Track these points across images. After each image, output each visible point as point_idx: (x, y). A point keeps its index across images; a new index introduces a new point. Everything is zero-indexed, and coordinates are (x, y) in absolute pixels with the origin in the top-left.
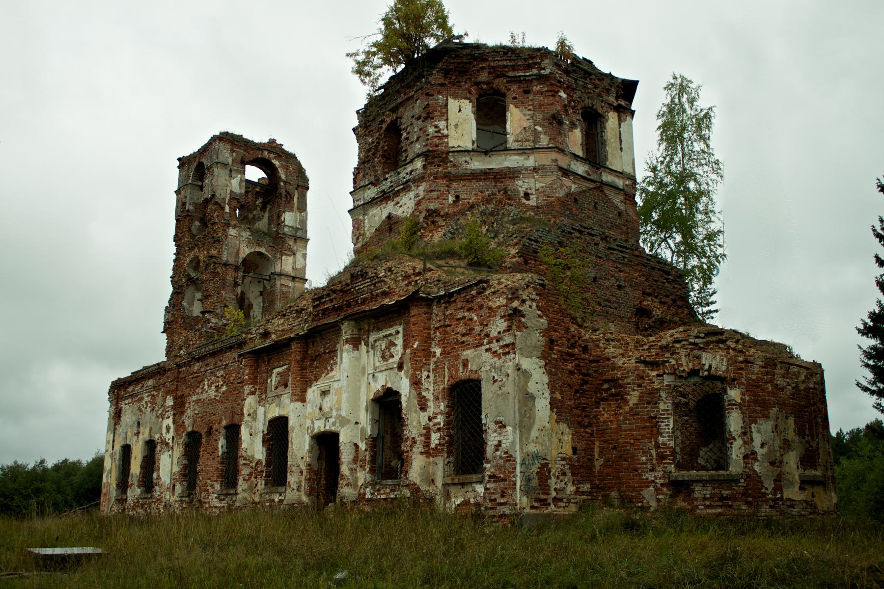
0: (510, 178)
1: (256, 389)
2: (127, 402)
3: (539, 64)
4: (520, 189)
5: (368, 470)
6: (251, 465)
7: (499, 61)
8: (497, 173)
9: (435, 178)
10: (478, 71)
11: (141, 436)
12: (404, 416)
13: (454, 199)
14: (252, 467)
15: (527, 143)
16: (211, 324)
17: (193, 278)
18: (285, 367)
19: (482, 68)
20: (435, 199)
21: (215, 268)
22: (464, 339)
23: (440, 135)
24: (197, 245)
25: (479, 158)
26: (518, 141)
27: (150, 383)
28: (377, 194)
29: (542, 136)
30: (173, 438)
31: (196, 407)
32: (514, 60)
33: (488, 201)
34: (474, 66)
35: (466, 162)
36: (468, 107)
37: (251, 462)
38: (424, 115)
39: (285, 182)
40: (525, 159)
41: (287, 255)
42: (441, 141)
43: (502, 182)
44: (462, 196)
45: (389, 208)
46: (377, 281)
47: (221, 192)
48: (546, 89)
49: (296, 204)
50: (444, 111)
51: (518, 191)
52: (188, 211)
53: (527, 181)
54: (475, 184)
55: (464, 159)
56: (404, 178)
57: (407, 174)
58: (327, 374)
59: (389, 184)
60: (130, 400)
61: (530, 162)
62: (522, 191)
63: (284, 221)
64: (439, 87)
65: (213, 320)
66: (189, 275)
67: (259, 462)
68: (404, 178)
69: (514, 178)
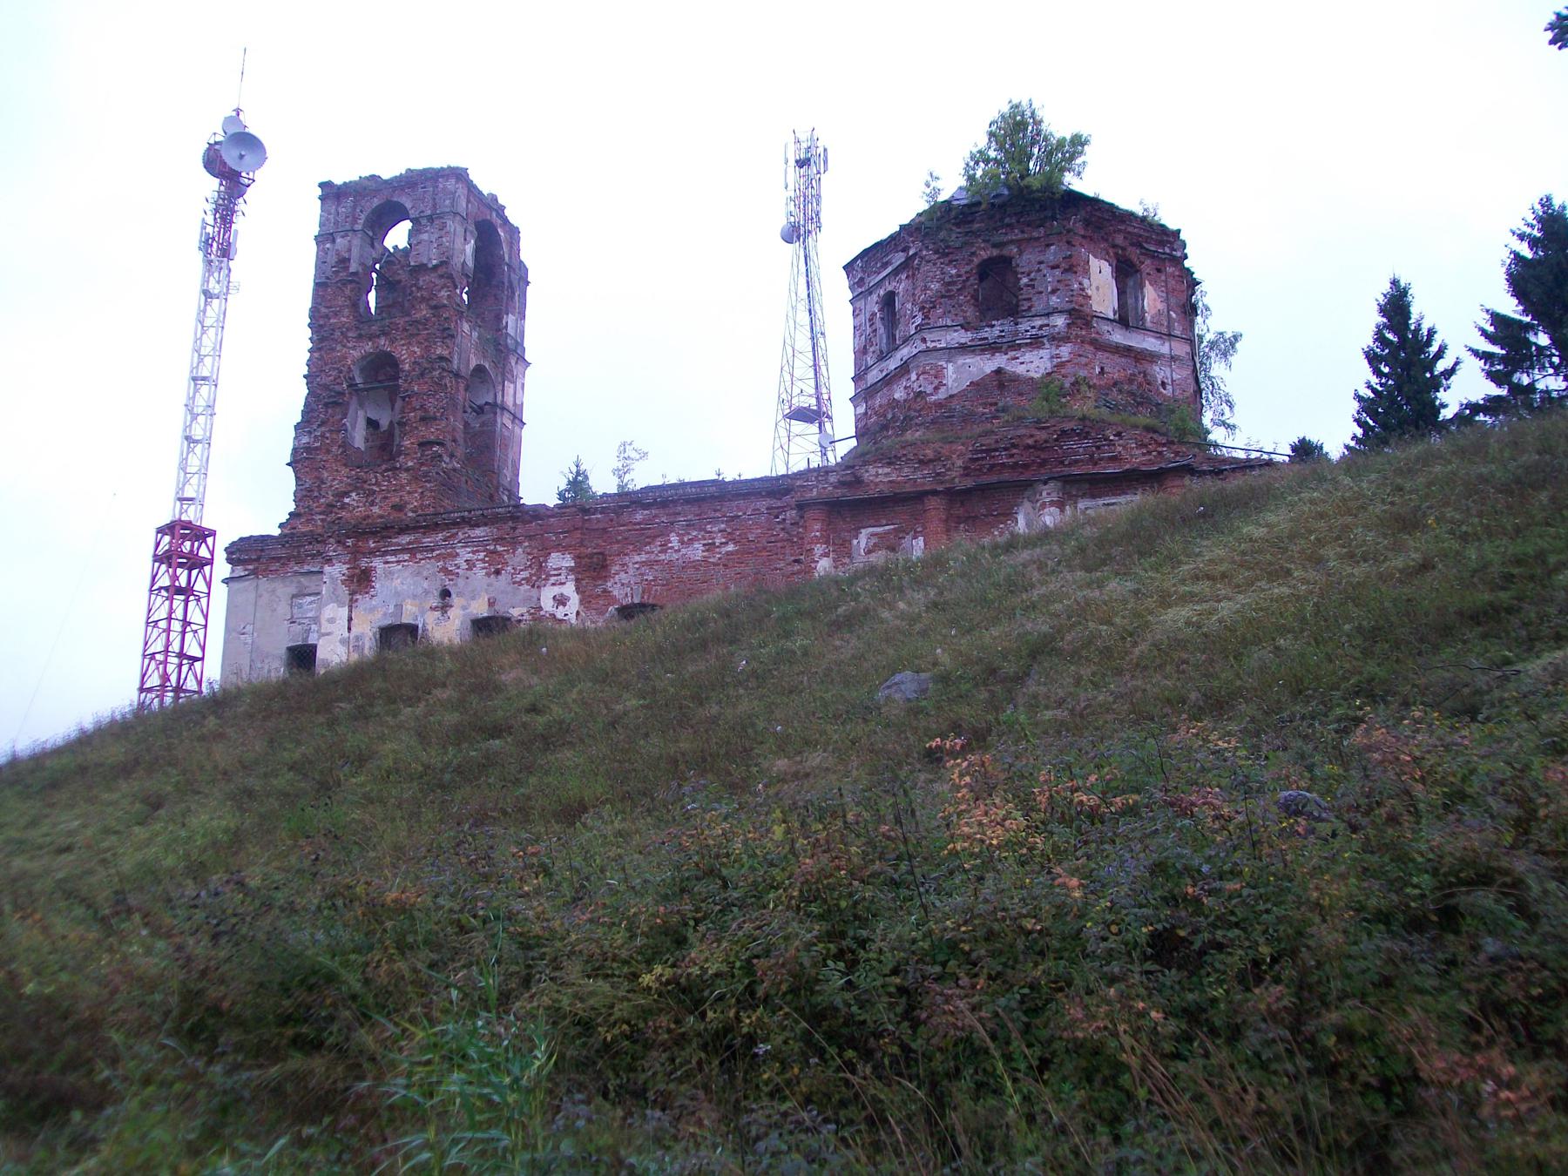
2: (390, 558)
9: (1082, 342)
19: (1120, 231)
21: (442, 378)
28: (972, 340)
30: (578, 613)
33: (1131, 381)
36: (1107, 269)
44: (1106, 369)
45: (999, 361)
57: (1033, 327)
59: (997, 333)
61: (1164, 349)
62: (1159, 378)
66: (353, 379)
69: (1152, 362)
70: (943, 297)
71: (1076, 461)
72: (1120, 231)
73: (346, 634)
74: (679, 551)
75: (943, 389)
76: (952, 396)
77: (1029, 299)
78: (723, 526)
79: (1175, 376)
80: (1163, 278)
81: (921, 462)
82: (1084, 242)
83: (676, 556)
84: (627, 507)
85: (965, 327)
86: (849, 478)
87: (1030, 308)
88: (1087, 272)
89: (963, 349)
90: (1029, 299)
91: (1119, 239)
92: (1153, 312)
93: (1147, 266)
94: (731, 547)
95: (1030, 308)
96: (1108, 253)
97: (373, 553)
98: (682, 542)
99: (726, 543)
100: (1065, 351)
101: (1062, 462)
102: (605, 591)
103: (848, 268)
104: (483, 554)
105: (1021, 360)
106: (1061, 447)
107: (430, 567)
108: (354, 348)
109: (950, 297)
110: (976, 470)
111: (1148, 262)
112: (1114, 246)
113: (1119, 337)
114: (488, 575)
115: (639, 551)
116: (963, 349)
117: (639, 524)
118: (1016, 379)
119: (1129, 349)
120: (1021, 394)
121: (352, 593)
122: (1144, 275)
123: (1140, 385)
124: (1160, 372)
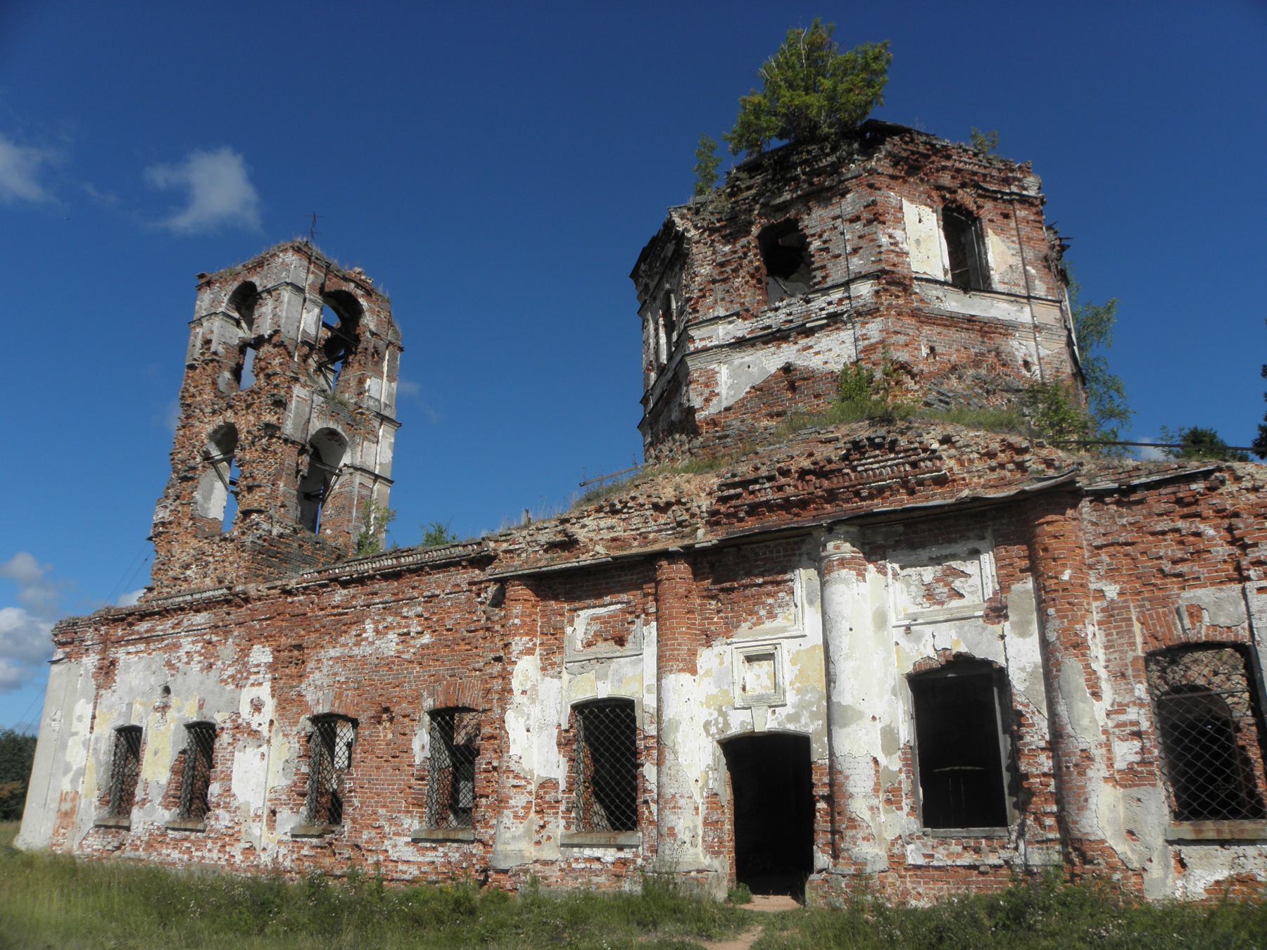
0: (1001, 334)
1: (535, 645)
2: (131, 649)
3: (1019, 180)
4: (1016, 353)
5: (906, 809)
6: (529, 788)
7: (966, 163)
8: (986, 323)
10: (938, 171)
11: (171, 714)
12: (1020, 708)
13: (928, 351)
14: (530, 793)
15: (1016, 288)
16: (260, 532)
17: (213, 458)
18: (619, 606)
19: (944, 168)
20: (902, 346)
22: (1180, 568)
23: (898, 250)
24: (231, 407)
25: (957, 297)
26: (1004, 283)
27: (201, 618)
28: (752, 332)
29: (1037, 282)
30: (272, 722)
31: (339, 669)
32: (985, 167)
34: (933, 162)
35: (938, 298)
37: (529, 783)
38: (865, 215)
39: (373, 334)
40: (1018, 311)
41: (370, 441)
42: (901, 259)
43: (990, 338)
44: (939, 349)
45: (788, 353)
46: (919, 455)
47: (290, 328)
48: (1032, 218)
49: (385, 369)
50: (900, 215)
51: (1014, 356)
52: (215, 353)
53: (1024, 343)
54: (953, 334)
55: (935, 293)
56: (822, 309)
57: (830, 303)
58: (755, 624)
60: (142, 647)
61: (1024, 315)
63: (369, 390)
64: (887, 179)
65: (265, 526)
67: (547, 784)
68: (822, 309)
70: (714, 282)
71: (881, 491)
72: (944, 168)
73: (88, 735)
74: (373, 643)
75: (715, 401)
76: (727, 409)
77: (823, 267)
78: (419, 609)
79: (1043, 352)
80: (1013, 224)
81: (656, 507)
82: (893, 183)
83: (369, 650)
84: (326, 586)
85: (743, 314)
86: (560, 538)
87: (824, 278)
88: (899, 221)
89: (740, 343)
90: (823, 267)
91: (946, 179)
92: (1003, 268)
93: (988, 210)
94: (426, 639)
95: (824, 278)
96: (929, 197)
97: (118, 642)
98: (377, 631)
99: (421, 633)
100: (874, 329)
101: (857, 494)
102: (300, 695)
103: (631, 276)
104: (201, 644)
105: (816, 349)
106: (854, 469)
107: (159, 658)
108: (209, 423)
109: (724, 281)
110: (728, 516)
111: (989, 205)
112: (939, 188)
113: (956, 303)
114: (202, 670)
115: (334, 642)
116: (740, 343)
117: (338, 607)
118: (810, 376)
119: (971, 320)
120: (817, 396)
121: (99, 687)
122: (985, 223)
123: (993, 368)
124: (1021, 348)
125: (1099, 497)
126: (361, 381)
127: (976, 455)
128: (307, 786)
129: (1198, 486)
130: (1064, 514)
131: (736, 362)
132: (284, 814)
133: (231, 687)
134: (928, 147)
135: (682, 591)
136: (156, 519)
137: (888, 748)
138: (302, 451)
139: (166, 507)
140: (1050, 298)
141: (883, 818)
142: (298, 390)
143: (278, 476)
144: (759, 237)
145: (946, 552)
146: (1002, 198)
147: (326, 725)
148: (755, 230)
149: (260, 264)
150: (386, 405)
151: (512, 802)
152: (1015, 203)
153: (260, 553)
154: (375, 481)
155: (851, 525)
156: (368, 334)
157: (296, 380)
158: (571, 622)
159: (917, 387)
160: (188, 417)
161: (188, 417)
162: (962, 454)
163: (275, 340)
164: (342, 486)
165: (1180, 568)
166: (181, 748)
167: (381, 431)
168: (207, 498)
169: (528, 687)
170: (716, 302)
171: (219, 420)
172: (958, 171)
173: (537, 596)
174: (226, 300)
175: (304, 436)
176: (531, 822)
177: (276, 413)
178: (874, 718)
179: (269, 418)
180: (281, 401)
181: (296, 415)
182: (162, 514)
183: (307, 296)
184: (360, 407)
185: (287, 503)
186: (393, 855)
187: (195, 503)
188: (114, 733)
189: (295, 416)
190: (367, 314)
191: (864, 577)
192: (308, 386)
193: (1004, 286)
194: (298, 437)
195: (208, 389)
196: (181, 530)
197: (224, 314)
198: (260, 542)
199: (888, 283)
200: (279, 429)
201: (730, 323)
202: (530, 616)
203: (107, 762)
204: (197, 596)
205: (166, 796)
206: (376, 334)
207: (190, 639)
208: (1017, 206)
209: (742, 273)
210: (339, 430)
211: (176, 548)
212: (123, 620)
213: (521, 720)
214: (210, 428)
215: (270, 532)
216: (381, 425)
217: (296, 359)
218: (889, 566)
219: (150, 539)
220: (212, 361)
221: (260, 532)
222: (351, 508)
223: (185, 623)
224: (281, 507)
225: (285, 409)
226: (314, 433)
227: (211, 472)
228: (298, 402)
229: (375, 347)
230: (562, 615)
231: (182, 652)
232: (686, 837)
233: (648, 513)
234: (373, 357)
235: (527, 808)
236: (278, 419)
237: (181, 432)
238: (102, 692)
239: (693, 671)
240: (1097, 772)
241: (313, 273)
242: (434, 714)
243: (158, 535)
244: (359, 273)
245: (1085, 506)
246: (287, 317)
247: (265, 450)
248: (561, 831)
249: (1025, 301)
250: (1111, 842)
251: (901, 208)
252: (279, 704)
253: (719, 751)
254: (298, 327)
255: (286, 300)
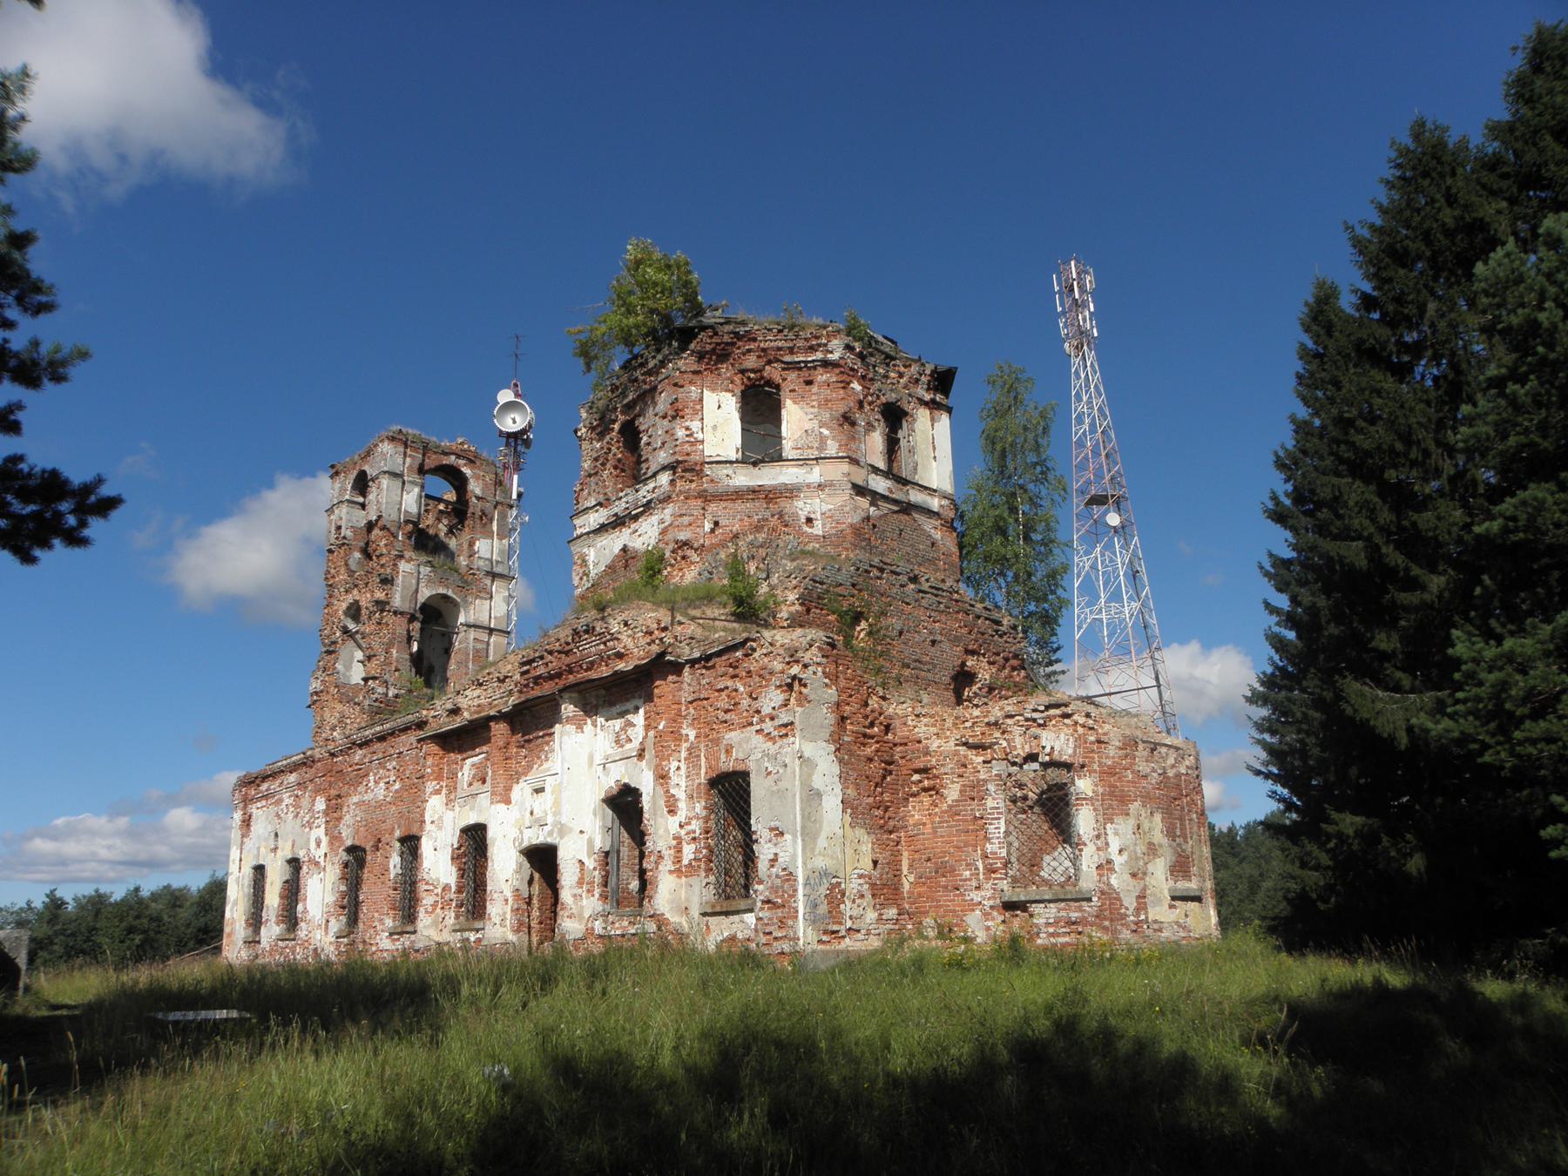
2: (259, 805)
4: (800, 512)
5: (597, 896)
6: (436, 891)
7: (771, 341)
10: (744, 354)
11: (279, 852)
14: (437, 895)
16: (376, 695)
19: (749, 351)
20: (686, 526)
22: (728, 717)
24: (356, 586)
32: (792, 340)
39: (478, 498)
40: (807, 472)
41: (482, 598)
49: (495, 528)
53: (809, 501)
55: (725, 471)
60: (264, 803)
61: (815, 475)
64: (690, 376)
65: (381, 690)
67: (446, 888)
68: (644, 497)
72: (749, 351)
89: (602, 529)
125: (693, 663)
126: (471, 544)
127: (641, 634)
128: (345, 900)
129: (739, 654)
130: (665, 680)
131: (599, 545)
132: (333, 921)
133: (308, 829)
134: (732, 336)
135: (501, 744)
136: (311, 689)
137: (591, 852)
138: (412, 619)
139: (317, 678)
140: (840, 455)
141: (585, 902)
142: (403, 566)
143: (389, 645)
144: (621, 431)
145: (624, 709)
146: (806, 366)
147: (355, 851)
148: (616, 426)
149: (368, 454)
150: (497, 562)
151: (424, 902)
152: (819, 368)
153: (377, 713)
154: (490, 634)
155: (571, 692)
156: (474, 499)
157: (401, 557)
158: (462, 768)
159: (698, 559)
160: (331, 597)
161: (331, 597)
162: (635, 633)
163: (380, 523)
164: (460, 643)
165: (728, 717)
166: (285, 879)
167: (494, 587)
168: (348, 667)
169: (435, 818)
170: (589, 494)
171: (350, 598)
172: (764, 350)
173: (444, 749)
174: (349, 487)
175: (413, 606)
176: (438, 915)
177: (384, 590)
178: (581, 832)
179: (380, 595)
180: (387, 579)
181: (404, 588)
182: (315, 685)
183: (406, 478)
184: (471, 569)
185: (400, 667)
186: (381, 946)
187: (338, 673)
188: (252, 871)
189: (402, 589)
190: (471, 480)
191: (582, 728)
192: (412, 560)
193: (796, 452)
194: (406, 607)
195: (343, 570)
196: (330, 697)
197: (349, 501)
198: (376, 704)
199: (683, 471)
200: (388, 603)
201: (597, 511)
202: (438, 765)
203: (249, 894)
204: (288, 761)
205: (277, 916)
206: (482, 498)
207: (288, 794)
208: (820, 370)
209: (608, 466)
210: (450, 593)
211: (327, 715)
212: (253, 782)
213: (431, 843)
214: (344, 606)
215: (387, 695)
216: (493, 581)
217: (400, 538)
218: (599, 720)
219: (309, 706)
220: (343, 544)
221: (376, 695)
222: (467, 662)
223: (285, 782)
224: (396, 670)
225: (392, 585)
226: (423, 601)
227: (351, 643)
228: (403, 576)
229: (482, 511)
230: (457, 763)
231: (283, 806)
232: (497, 920)
233: (495, 684)
234: (482, 520)
235: (435, 905)
236: (387, 594)
237: (326, 611)
238: (245, 840)
239: (508, 802)
240: (667, 865)
241: (410, 456)
242: (402, 840)
243: (314, 702)
244: (462, 444)
245: (687, 669)
246: (387, 503)
247: (379, 624)
248: (452, 921)
249: (815, 462)
250: (667, 915)
251: (701, 400)
252: (330, 841)
253: (522, 859)
254: (399, 510)
255: (385, 487)
